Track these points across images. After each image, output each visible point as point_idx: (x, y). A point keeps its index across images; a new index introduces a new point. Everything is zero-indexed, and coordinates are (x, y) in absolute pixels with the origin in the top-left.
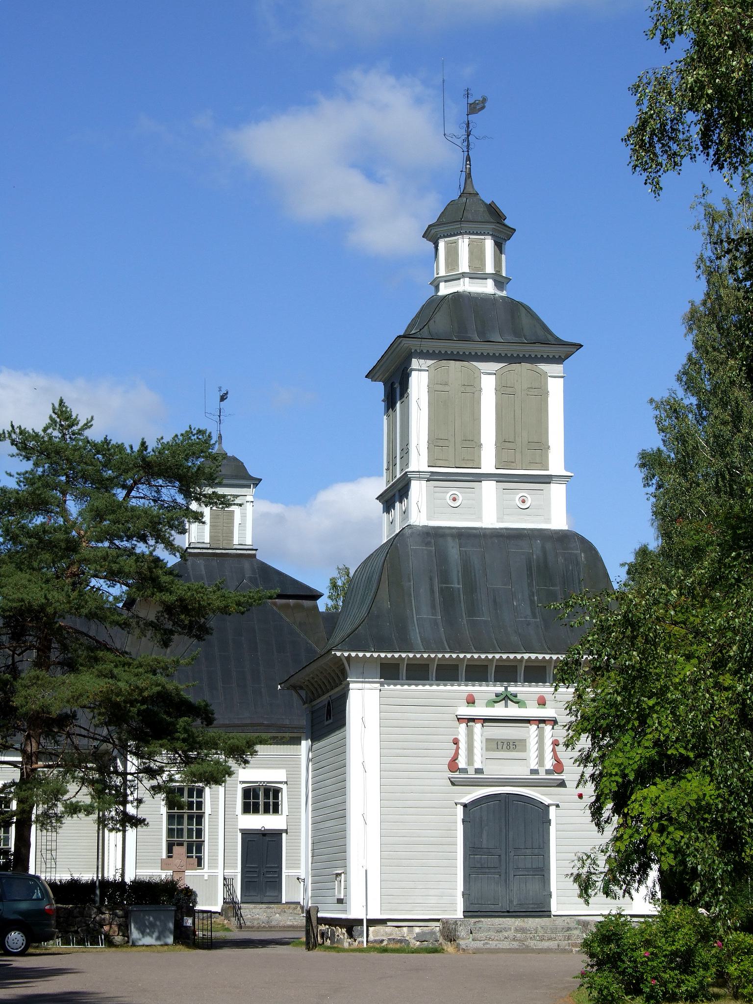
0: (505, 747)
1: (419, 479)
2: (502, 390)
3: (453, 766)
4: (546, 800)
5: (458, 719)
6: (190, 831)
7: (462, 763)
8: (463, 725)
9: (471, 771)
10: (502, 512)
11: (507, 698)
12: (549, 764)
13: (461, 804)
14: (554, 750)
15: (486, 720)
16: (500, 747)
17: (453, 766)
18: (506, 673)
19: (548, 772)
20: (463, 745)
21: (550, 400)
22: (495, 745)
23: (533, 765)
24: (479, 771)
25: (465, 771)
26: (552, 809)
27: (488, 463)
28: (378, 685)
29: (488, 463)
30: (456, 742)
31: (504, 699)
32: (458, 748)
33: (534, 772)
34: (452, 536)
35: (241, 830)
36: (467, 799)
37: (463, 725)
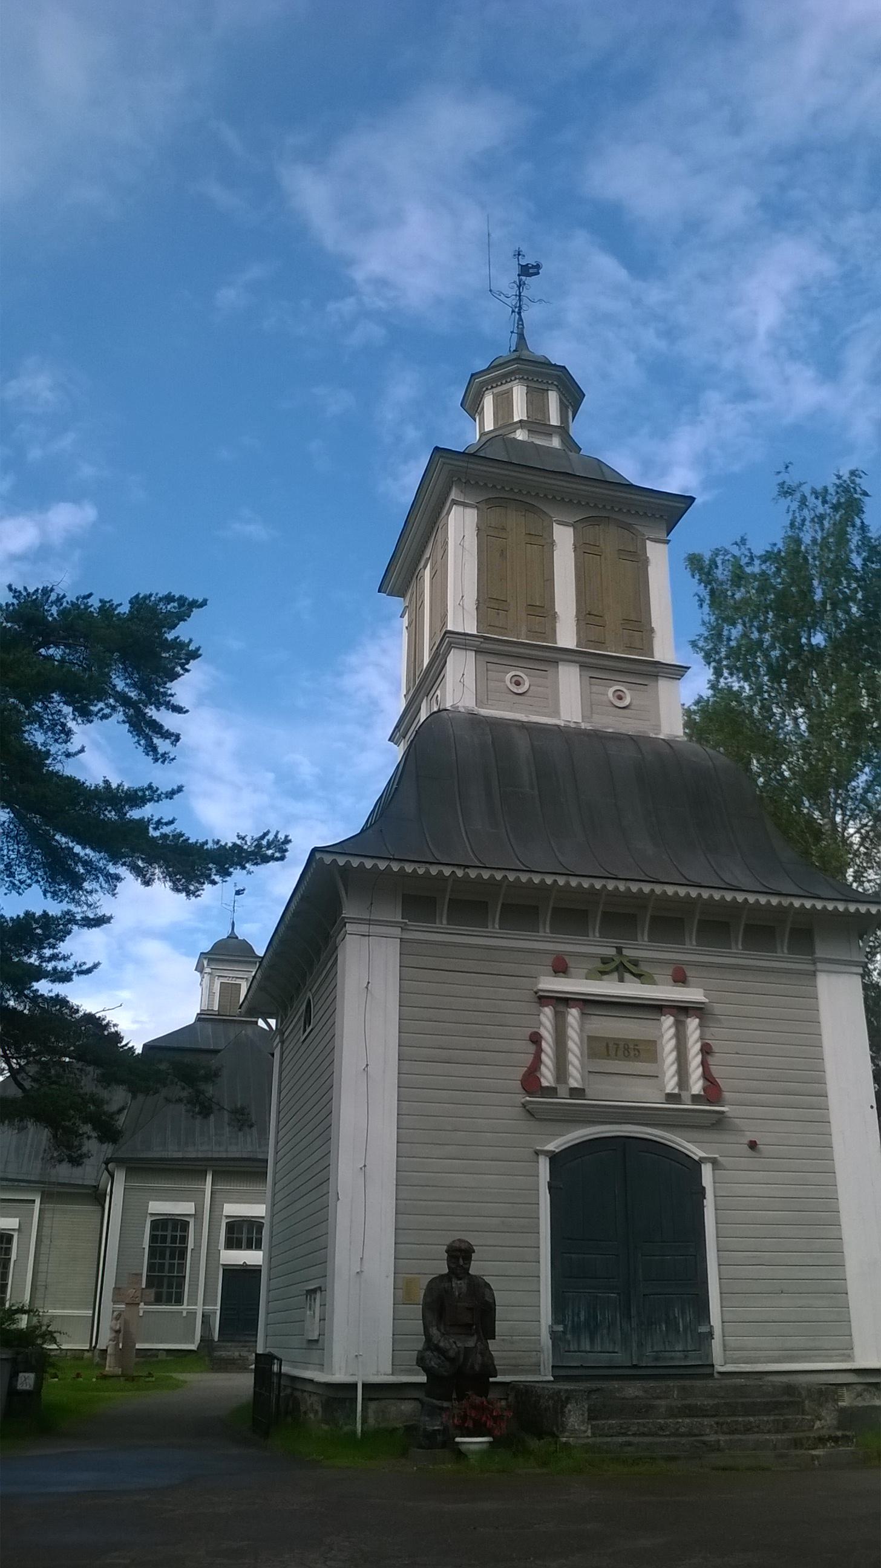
0: (620, 1053)
1: (465, 647)
2: (582, 549)
3: (530, 1082)
4: (696, 1152)
5: (540, 998)
6: (172, 1265)
7: (547, 1078)
8: (548, 1011)
9: (562, 1091)
10: (589, 706)
11: (623, 968)
12: (697, 1086)
13: (546, 1153)
14: (704, 1064)
15: (589, 1004)
16: (612, 1052)
17: (530, 1082)
18: (622, 917)
19: (696, 1099)
20: (548, 1046)
21: (652, 570)
22: (601, 1049)
23: (671, 1085)
24: (576, 1093)
25: (551, 1092)
26: (707, 1171)
27: (566, 636)
28: (397, 931)
29: (566, 636)
30: (536, 1039)
31: (616, 969)
32: (539, 1051)
33: (671, 1098)
34: (516, 726)
35: (224, 1265)
36: (554, 1145)
37: (548, 1011)
